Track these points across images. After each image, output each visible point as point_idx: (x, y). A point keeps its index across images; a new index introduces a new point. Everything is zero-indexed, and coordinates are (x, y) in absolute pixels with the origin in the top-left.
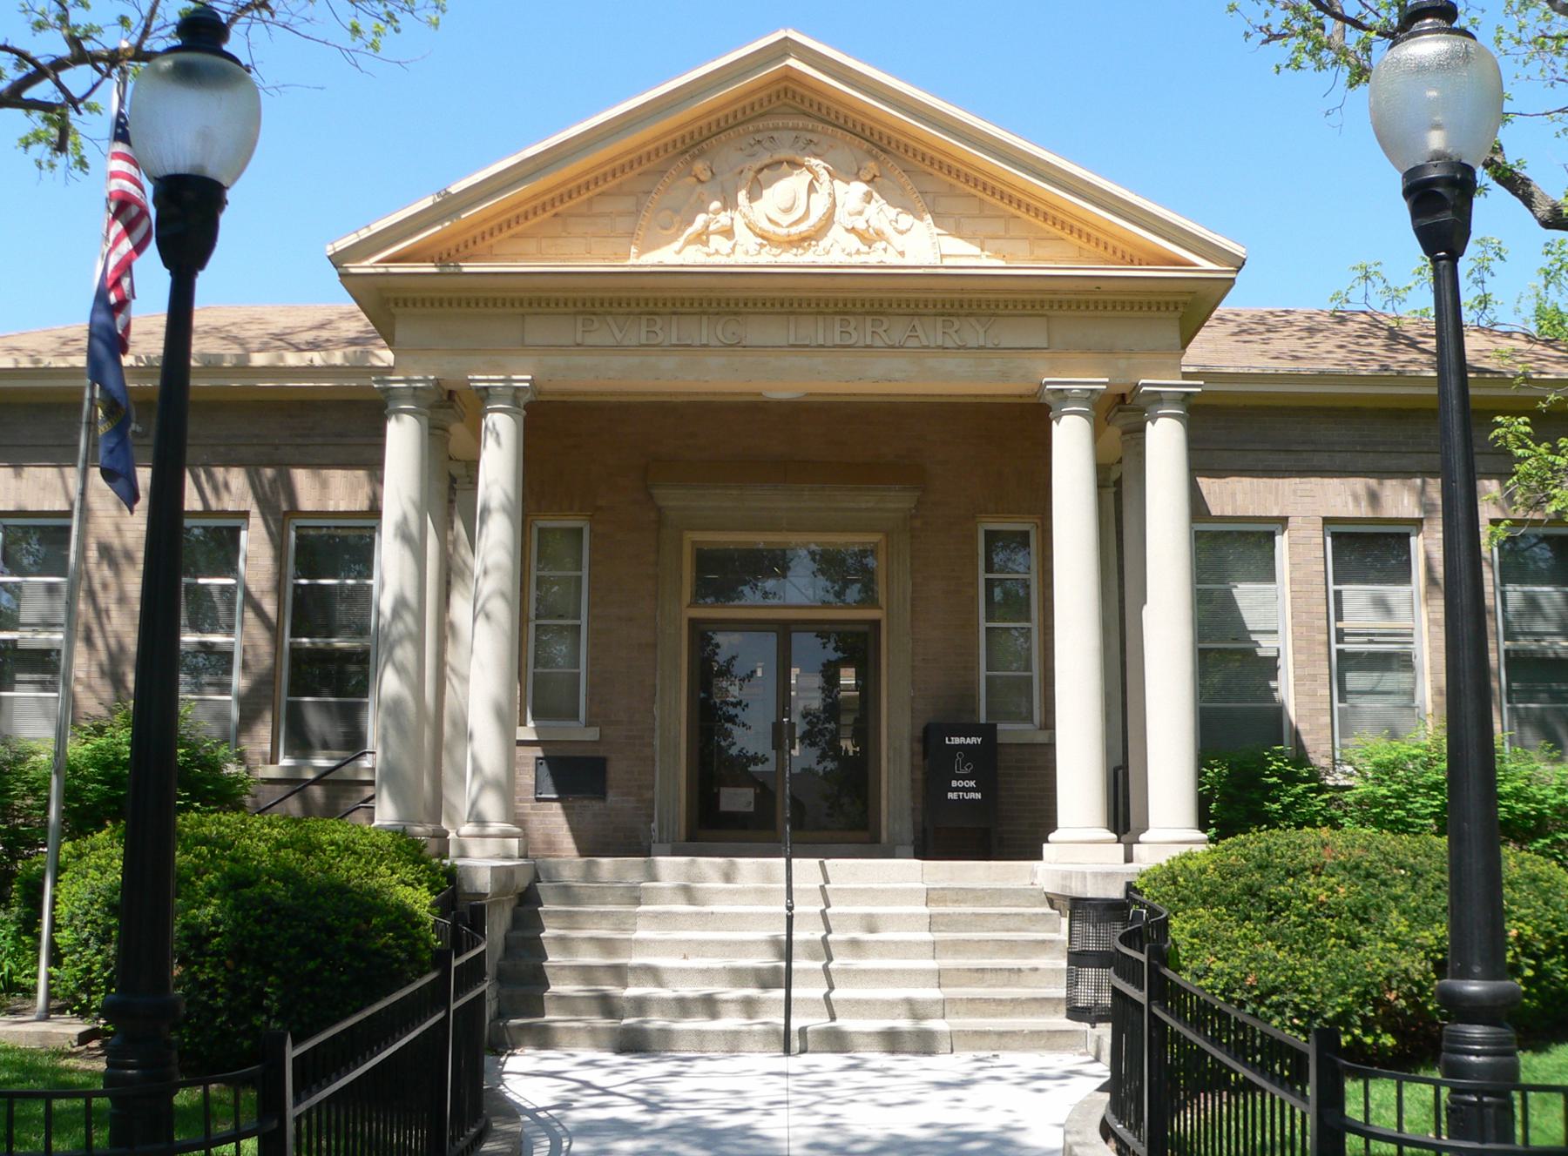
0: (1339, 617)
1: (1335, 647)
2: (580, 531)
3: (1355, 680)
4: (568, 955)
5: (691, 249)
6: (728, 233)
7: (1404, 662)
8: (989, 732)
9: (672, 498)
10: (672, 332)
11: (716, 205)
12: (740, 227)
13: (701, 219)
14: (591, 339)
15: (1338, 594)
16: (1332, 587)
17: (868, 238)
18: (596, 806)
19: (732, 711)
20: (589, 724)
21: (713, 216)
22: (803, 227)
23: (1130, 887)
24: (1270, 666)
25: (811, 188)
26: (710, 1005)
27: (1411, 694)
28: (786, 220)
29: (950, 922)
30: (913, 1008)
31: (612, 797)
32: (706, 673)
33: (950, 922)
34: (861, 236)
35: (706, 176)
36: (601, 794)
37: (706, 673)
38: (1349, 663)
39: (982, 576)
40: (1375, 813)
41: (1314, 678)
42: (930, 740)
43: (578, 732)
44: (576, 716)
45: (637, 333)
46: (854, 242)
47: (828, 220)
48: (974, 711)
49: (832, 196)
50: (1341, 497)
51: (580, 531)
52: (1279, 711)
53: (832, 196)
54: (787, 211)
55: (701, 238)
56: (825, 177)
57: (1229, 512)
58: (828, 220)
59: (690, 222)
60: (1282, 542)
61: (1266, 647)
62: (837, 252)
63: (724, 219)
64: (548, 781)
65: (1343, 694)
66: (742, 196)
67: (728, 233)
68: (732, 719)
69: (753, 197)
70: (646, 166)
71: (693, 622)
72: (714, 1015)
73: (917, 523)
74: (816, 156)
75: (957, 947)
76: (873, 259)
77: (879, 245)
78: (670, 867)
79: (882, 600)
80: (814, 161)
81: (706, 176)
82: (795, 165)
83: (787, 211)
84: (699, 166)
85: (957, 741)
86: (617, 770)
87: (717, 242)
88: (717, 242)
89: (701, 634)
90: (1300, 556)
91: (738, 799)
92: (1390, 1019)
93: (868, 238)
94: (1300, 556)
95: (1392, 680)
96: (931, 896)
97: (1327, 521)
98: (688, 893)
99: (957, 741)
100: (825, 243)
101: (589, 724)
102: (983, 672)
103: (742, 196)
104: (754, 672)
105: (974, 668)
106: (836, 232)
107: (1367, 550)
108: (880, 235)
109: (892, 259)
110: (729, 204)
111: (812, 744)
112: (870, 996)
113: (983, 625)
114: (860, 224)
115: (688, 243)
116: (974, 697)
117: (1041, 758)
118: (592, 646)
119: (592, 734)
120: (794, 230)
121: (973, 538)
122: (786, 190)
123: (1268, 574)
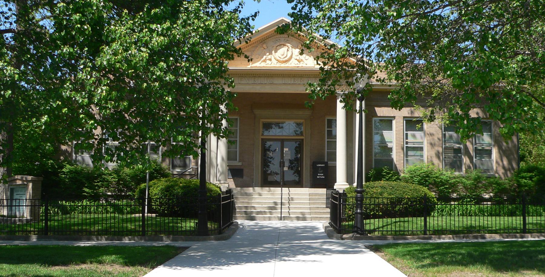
0: (407, 139)
1: (405, 145)
2: (237, 119)
3: (410, 153)
4: (239, 204)
5: (263, 63)
6: (270, 60)
7: (421, 149)
8: (326, 163)
9: (257, 112)
10: (259, 81)
11: (268, 54)
12: (273, 59)
13: (265, 57)
14: (242, 82)
15: (407, 134)
16: (405, 132)
17: (299, 61)
18: (241, 179)
19: (270, 160)
20: (239, 162)
21: (267, 56)
22: (286, 59)
23: (344, 191)
24: (391, 149)
25: (288, 50)
26: (265, 213)
27: (422, 156)
28: (282, 57)
29: (313, 199)
30: (303, 213)
31: (245, 178)
32: (265, 150)
33: (313, 199)
34: (298, 61)
35: (266, 48)
36: (242, 176)
37: (265, 150)
38: (407, 150)
39: (326, 129)
40: (406, 181)
41: (400, 152)
42: (314, 165)
43: (237, 163)
44: (236, 160)
45: (251, 81)
46: (296, 62)
47: (291, 57)
48: (324, 159)
49: (292, 52)
50: (406, 112)
51: (237, 119)
52: (392, 160)
53: (292, 52)
54: (283, 55)
55: (265, 61)
56: (291, 48)
57: (382, 115)
58: (291, 57)
59: (262, 58)
60: (394, 122)
61: (390, 145)
62: (293, 64)
63: (269, 57)
64: (230, 174)
65: (407, 156)
66: (273, 52)
67: (270, 60)
68: (270, 162)
69: (275, 52)
70: (253, 45)
71: (262, 139)
72: (266, 214)
73: (312, 117)
74: (289, 43)
75: (314, 203)
76: (300, 65)
77: (302, 62)
78: (258, 189)
79: (304, 135)
80: (288, 45)
81: (266, 48)
82: (284, 45)
83: (283, 55)
84: (264, 46)
85: (319, 165)
86: (245, 172)
87: (268, 62)
88: (268, 62)
89: (264, 141)
90: (398, 125)
91: (270, 178)
92: (382, 210)
93: (299, 61)
94: (398, 125)
95: (419, 153)
96: (310, 195)
97: (404, 117)
98: (260, 195)
99: (319, 165)
100: (290, 62)
101: (239, 162)
102: (326, 150)
103: (273, 52)
104: (276, 150)
105: (324, 149)
106: (293, 60)
107: (412, 124)
108: (302, 60)
109: (304, 65)
110: (271, 53)
111: (292, 169)
112: (296, 211)
113: (326, 140)
114: (298, 58)
115: (262, 62)
116: (324, 156)
117: (334, 168)
118: (240, 144)
119: (240, 164)
120: (284, 59)
121: (325, 120)
122: (282, 51)
123: (391, 129)
